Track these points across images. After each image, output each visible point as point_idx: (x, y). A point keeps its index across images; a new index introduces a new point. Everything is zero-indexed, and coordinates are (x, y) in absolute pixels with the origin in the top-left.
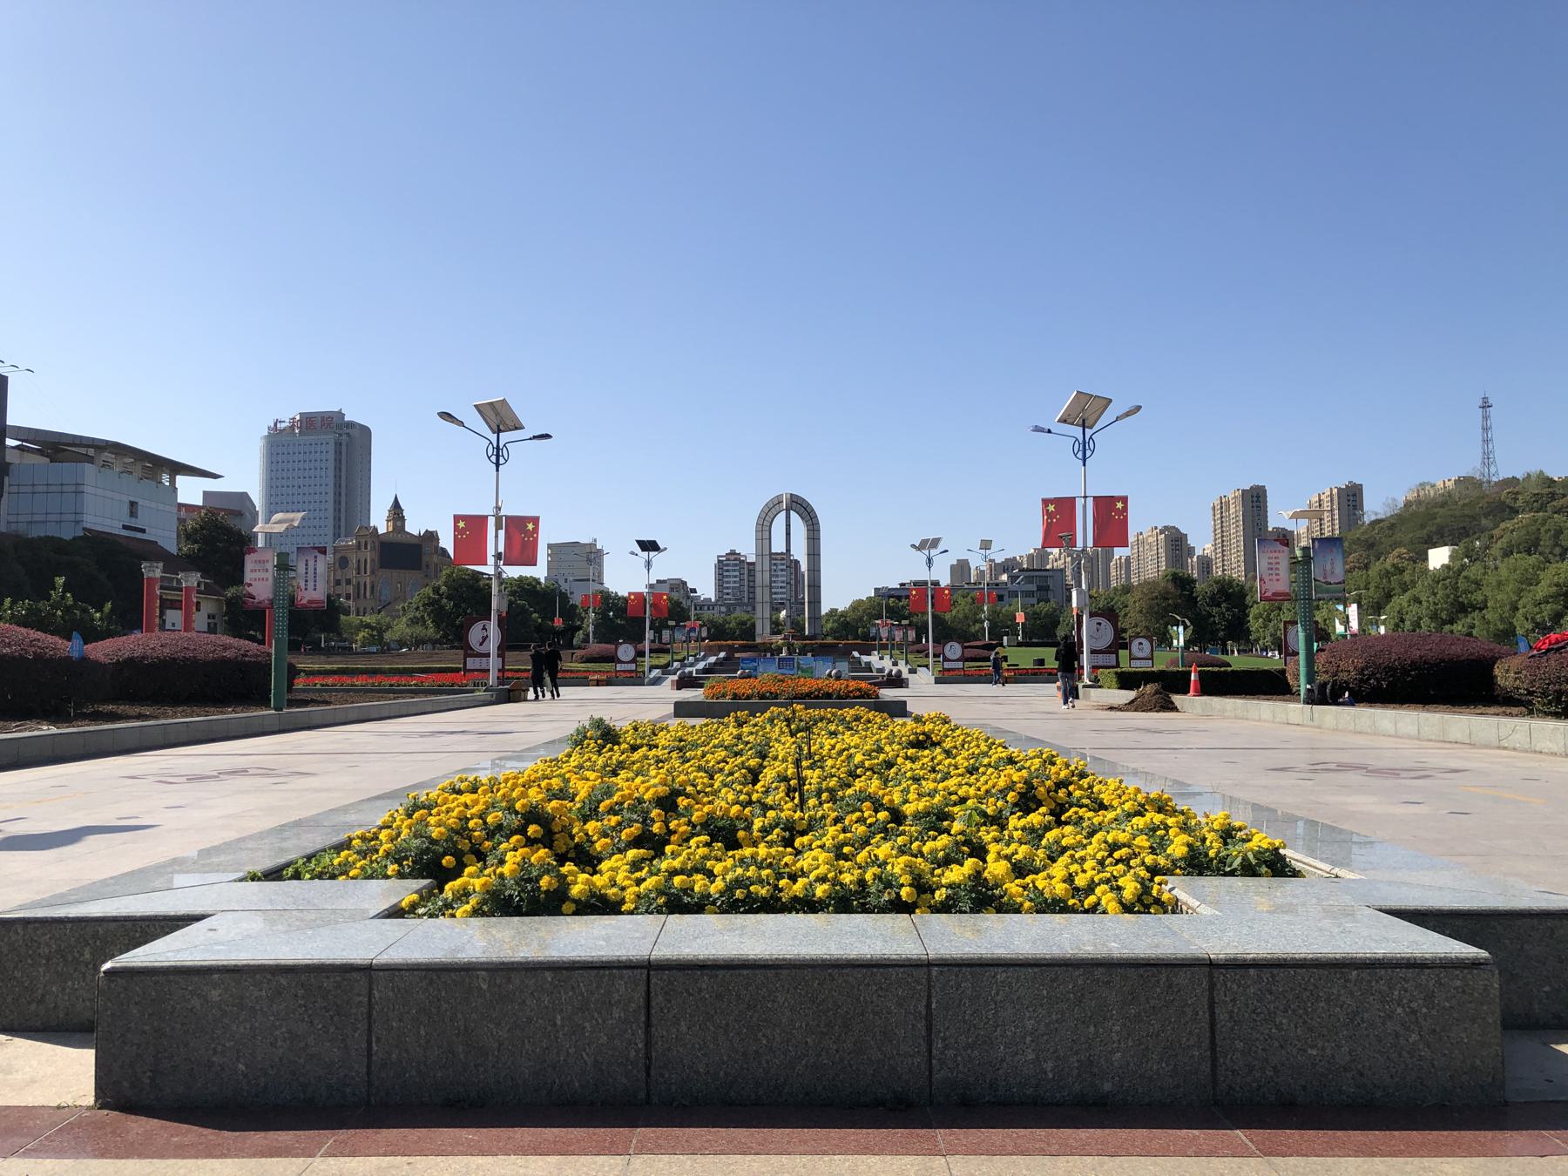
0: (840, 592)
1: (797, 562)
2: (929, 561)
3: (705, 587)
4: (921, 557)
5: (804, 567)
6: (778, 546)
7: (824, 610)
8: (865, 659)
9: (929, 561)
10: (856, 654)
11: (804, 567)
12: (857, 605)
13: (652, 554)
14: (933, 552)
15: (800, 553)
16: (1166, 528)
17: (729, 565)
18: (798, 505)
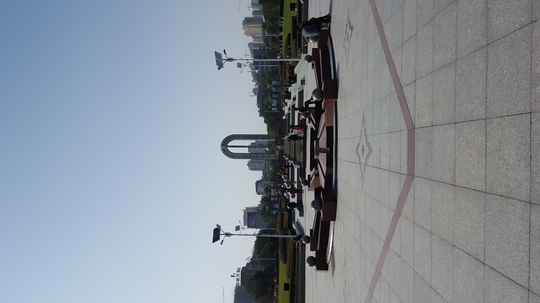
0: (261, 127)
1: (251, 144)
2: (230, 60)
3: (258, 175)
4: (226, 64)
5: (254, 141)
6: (246, 151)
7: (310, 18)
8: (286, 111)
9: (230, 60)
10: (284, 117)
11: (254, 141)
12: (265, 122)
13: (221, 232)
14: (224, 57)
15: (248, 142)
16: (243, 25)
17: (252, 167)
18: (225, 143)
